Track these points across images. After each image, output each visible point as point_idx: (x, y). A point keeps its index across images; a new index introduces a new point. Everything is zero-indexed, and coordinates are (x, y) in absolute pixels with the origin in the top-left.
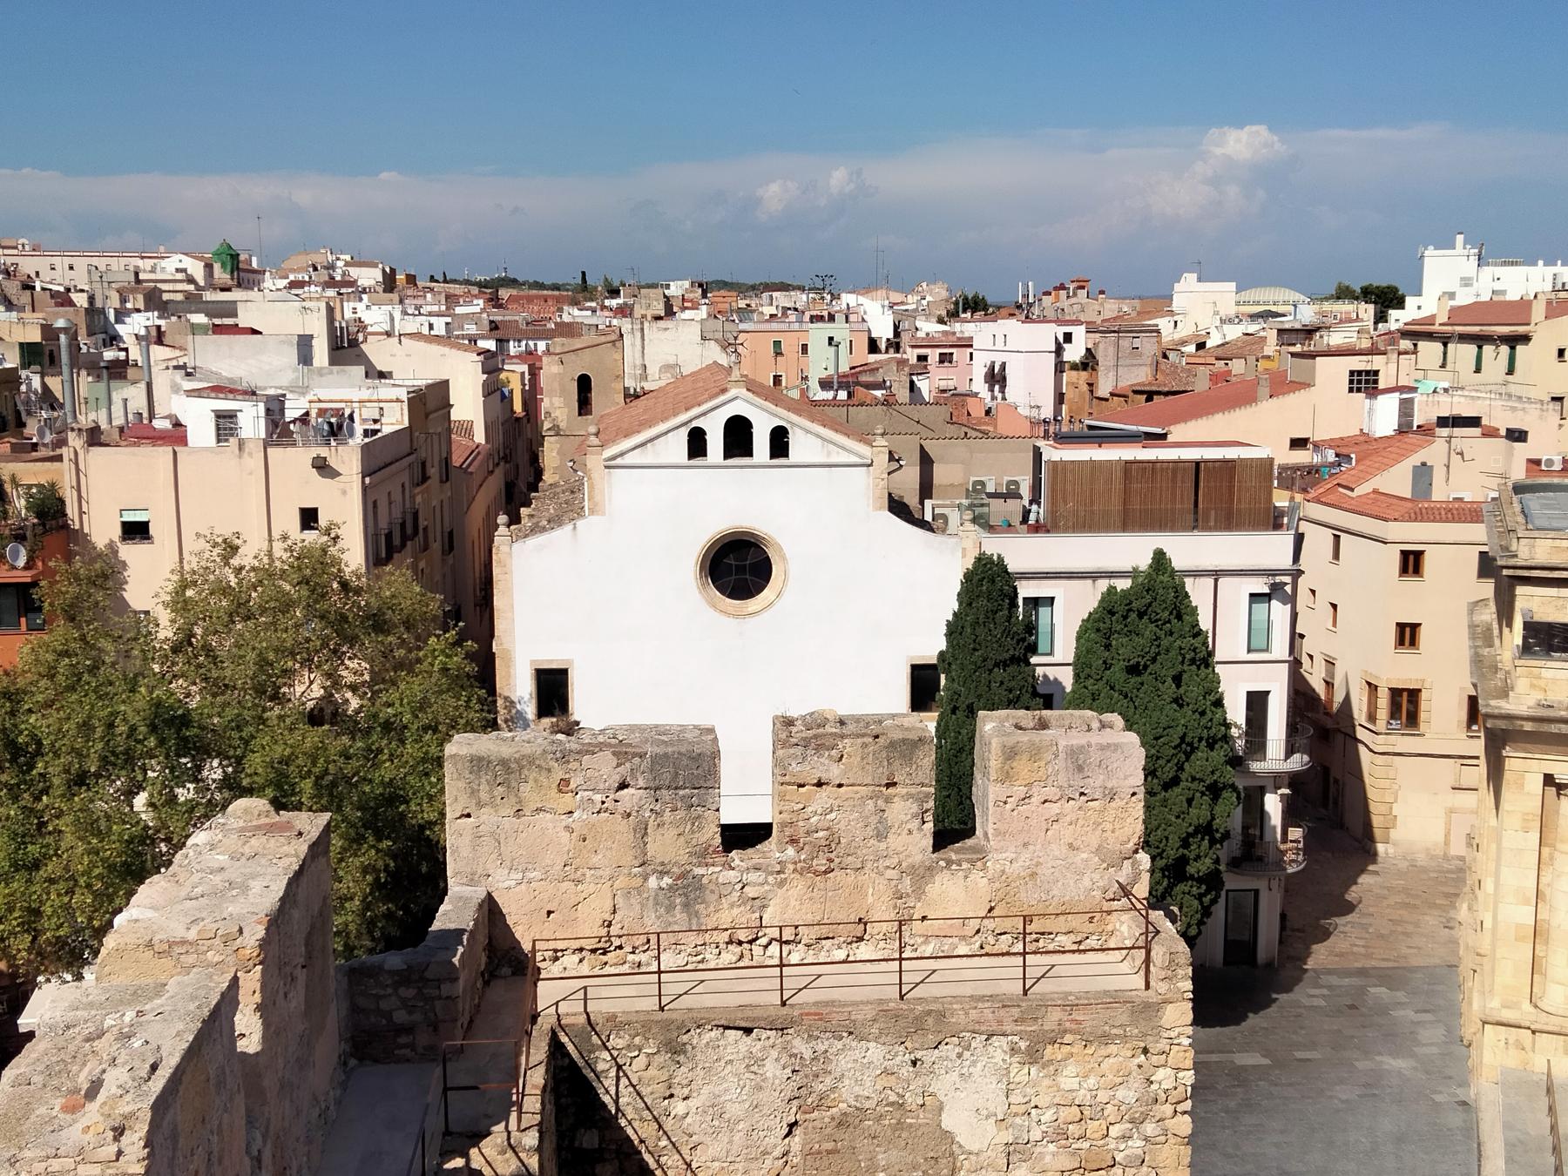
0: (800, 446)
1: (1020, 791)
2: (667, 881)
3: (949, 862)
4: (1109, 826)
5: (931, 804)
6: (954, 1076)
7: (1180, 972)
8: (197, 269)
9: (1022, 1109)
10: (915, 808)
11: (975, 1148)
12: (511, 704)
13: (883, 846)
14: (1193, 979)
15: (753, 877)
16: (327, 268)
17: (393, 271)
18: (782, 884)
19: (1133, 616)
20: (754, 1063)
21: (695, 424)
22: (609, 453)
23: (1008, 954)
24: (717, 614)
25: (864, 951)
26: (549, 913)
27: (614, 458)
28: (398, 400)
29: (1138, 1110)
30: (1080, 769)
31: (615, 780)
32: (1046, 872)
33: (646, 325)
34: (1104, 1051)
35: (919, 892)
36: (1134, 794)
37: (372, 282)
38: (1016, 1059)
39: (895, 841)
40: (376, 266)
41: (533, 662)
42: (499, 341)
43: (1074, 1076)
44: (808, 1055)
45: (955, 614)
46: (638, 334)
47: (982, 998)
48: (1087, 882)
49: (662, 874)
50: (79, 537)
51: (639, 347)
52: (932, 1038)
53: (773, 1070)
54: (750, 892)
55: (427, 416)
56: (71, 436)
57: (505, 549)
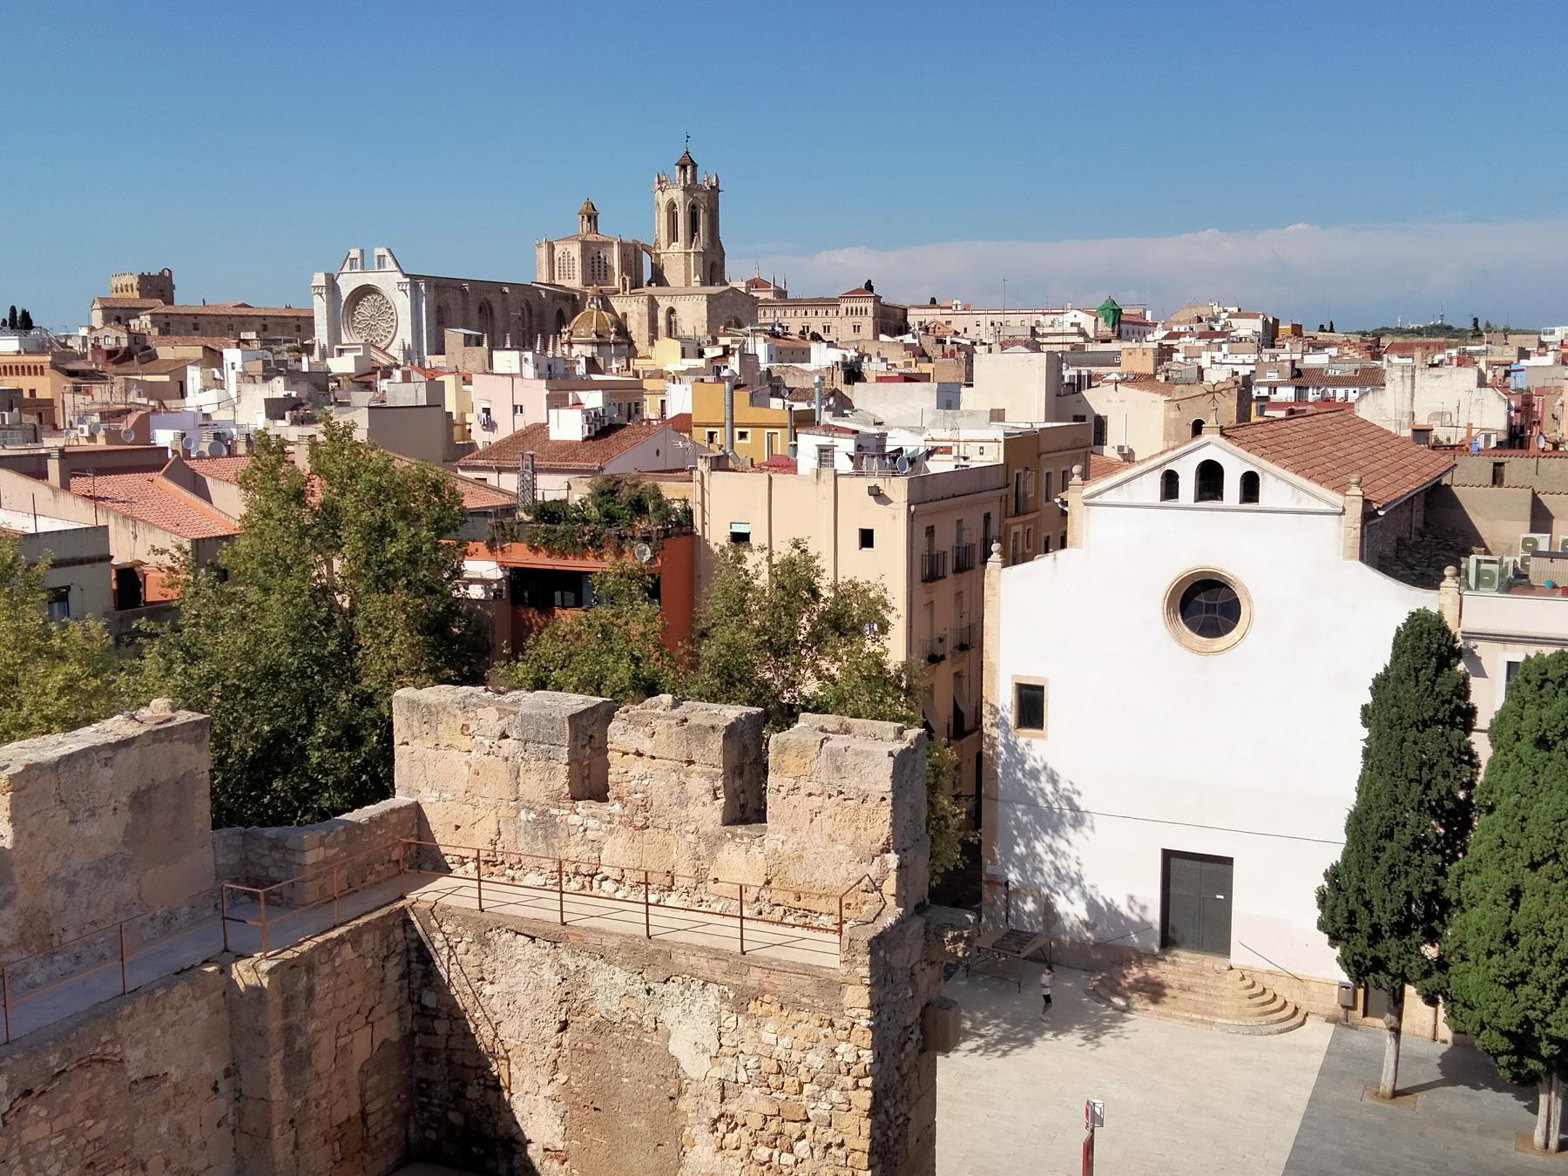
0: (1269, 491)
1: (790, 783)
2: (532, 816)
3: (734, 836)
4: (862, 825)
5: (720, 783)
6: (678, 1010)
7: (859, 958)
8: (1087, 322)
9: (731, 1052)
10: (708, 785)
11: (695, 1075)
12: (995, 711)
13: (684, 813)
14: (871, 966)
15: (591, 823)
16: (1210, 320)
17: (1276, 321)
18: (611, 831)
19: (1549, 686)
20: (536, 965)
21: (1168, 467)
22: (1088, 490)
23: (780, 923)
24: (1182, 650)
25: (672, 900)
26: (458, 827)
27: (1092, 496)
28: (996, 441)
29: (824, 1076)
30: (838, 769)
31: (497, 731)
32: (809, 855)
33: (1418, 372)
34: (795, 1016)
35: (712, 857)
36: (883, 799)
37: (1249, 333)
38: (724, 1006)
39: (694, 811)
40: (1256, 316)
41: (1014, 676)
42: (1298, 388)
43: (774, 1035)
44: (572, 968)
45: (1386, 668)
46: (1409, 382)
47: (702, 949)
48: (843, 871)
49: (530, 809)
50: (702, 541)
51: (1408, 395)
52: (662, 975)
53: (549, 975)
54: (590, 835)
55: (1039, 455)
56: (700, 462)
57: (994, 573)
